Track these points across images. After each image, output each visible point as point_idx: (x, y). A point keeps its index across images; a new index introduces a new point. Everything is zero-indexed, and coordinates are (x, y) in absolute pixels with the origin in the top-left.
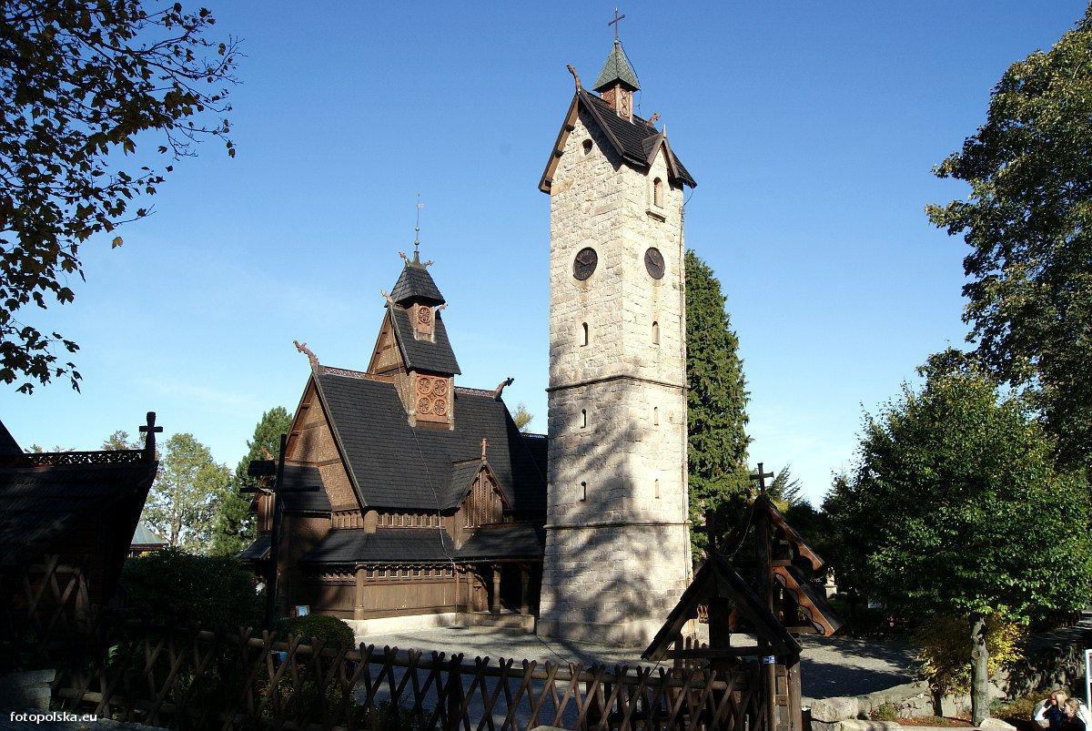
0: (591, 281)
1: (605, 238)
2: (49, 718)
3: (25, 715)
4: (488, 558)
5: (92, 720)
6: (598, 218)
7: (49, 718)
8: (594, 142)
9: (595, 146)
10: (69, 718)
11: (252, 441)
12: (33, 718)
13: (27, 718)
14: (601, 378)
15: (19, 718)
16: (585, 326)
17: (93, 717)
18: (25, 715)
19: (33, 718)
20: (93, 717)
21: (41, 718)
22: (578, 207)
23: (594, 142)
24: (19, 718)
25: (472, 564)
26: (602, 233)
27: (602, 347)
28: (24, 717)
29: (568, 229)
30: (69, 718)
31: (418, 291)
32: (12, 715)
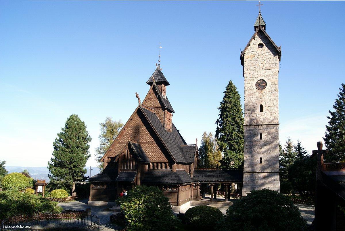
0: (263, 91)
1: (271, 77)
2: (16, 227)
3: (8, 226)
4: (218, 181)
5: (29, 227)
6: (268, 71)
7: (16, 227)
8: (264, 44)
9: (265, 46)
10: (22, 227)
11: (325, 138)
12: (10, 227)
13: (9, 227)
14: (271, 123)
15: (6, 227)
17: (29, 227)
18: (8, 226)
19: (10, 227)
20: (29, 227)
21: (13, 227)
22: (258, 65)
23: (264, 44)
24: (6, 227)
25: (228, 184)
27: (269, 114)
28: (7, 227)
29: (253, 71)
30: (22, 227)
31: (158, 83)
32: (4, 226)
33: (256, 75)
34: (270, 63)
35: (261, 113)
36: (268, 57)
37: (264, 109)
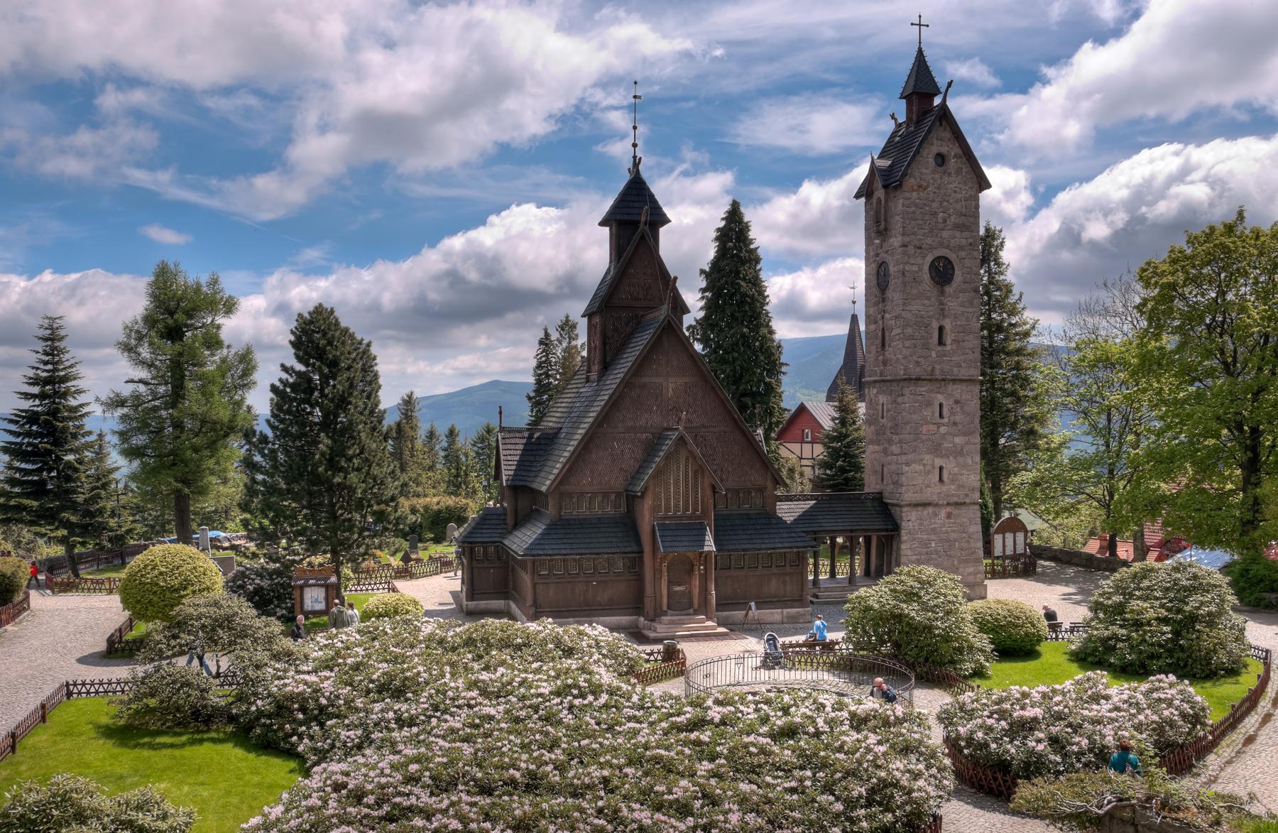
0: (948, 289)
1: (963, 254)
6: (958, 234)
16: (941, 329)
22: (935, 214)
26: (961, 248)
33: (929, 241)
34: (964, 211)
35: (940, 348)
36: (959, 196)
37: (948, 339)
